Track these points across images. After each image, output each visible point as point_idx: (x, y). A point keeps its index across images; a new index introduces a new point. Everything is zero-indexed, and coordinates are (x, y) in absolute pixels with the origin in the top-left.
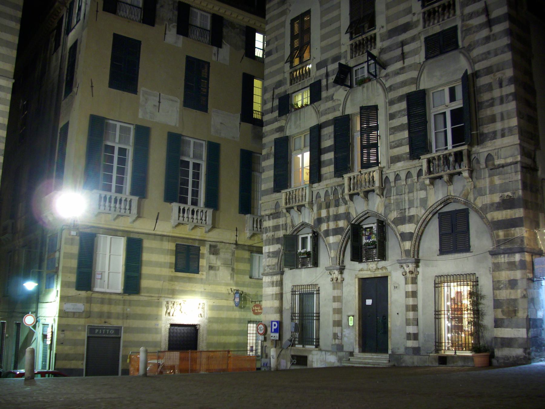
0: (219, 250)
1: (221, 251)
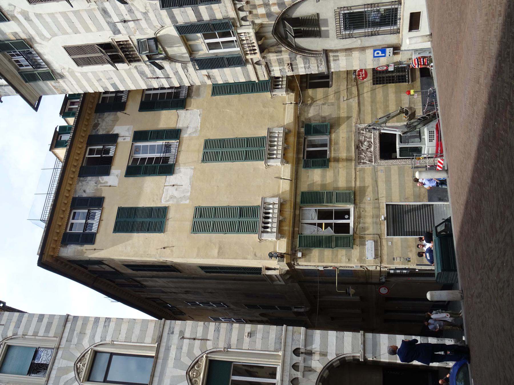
0: (306, 119)
1: (306, 117)
